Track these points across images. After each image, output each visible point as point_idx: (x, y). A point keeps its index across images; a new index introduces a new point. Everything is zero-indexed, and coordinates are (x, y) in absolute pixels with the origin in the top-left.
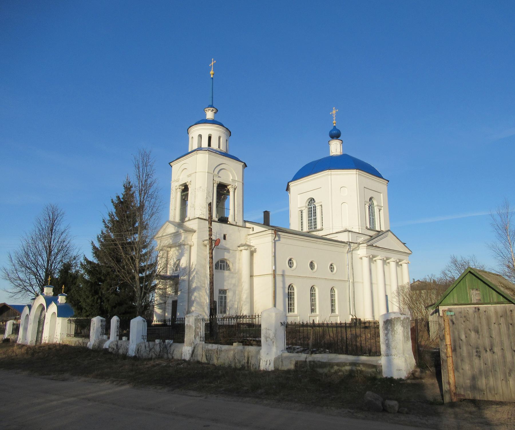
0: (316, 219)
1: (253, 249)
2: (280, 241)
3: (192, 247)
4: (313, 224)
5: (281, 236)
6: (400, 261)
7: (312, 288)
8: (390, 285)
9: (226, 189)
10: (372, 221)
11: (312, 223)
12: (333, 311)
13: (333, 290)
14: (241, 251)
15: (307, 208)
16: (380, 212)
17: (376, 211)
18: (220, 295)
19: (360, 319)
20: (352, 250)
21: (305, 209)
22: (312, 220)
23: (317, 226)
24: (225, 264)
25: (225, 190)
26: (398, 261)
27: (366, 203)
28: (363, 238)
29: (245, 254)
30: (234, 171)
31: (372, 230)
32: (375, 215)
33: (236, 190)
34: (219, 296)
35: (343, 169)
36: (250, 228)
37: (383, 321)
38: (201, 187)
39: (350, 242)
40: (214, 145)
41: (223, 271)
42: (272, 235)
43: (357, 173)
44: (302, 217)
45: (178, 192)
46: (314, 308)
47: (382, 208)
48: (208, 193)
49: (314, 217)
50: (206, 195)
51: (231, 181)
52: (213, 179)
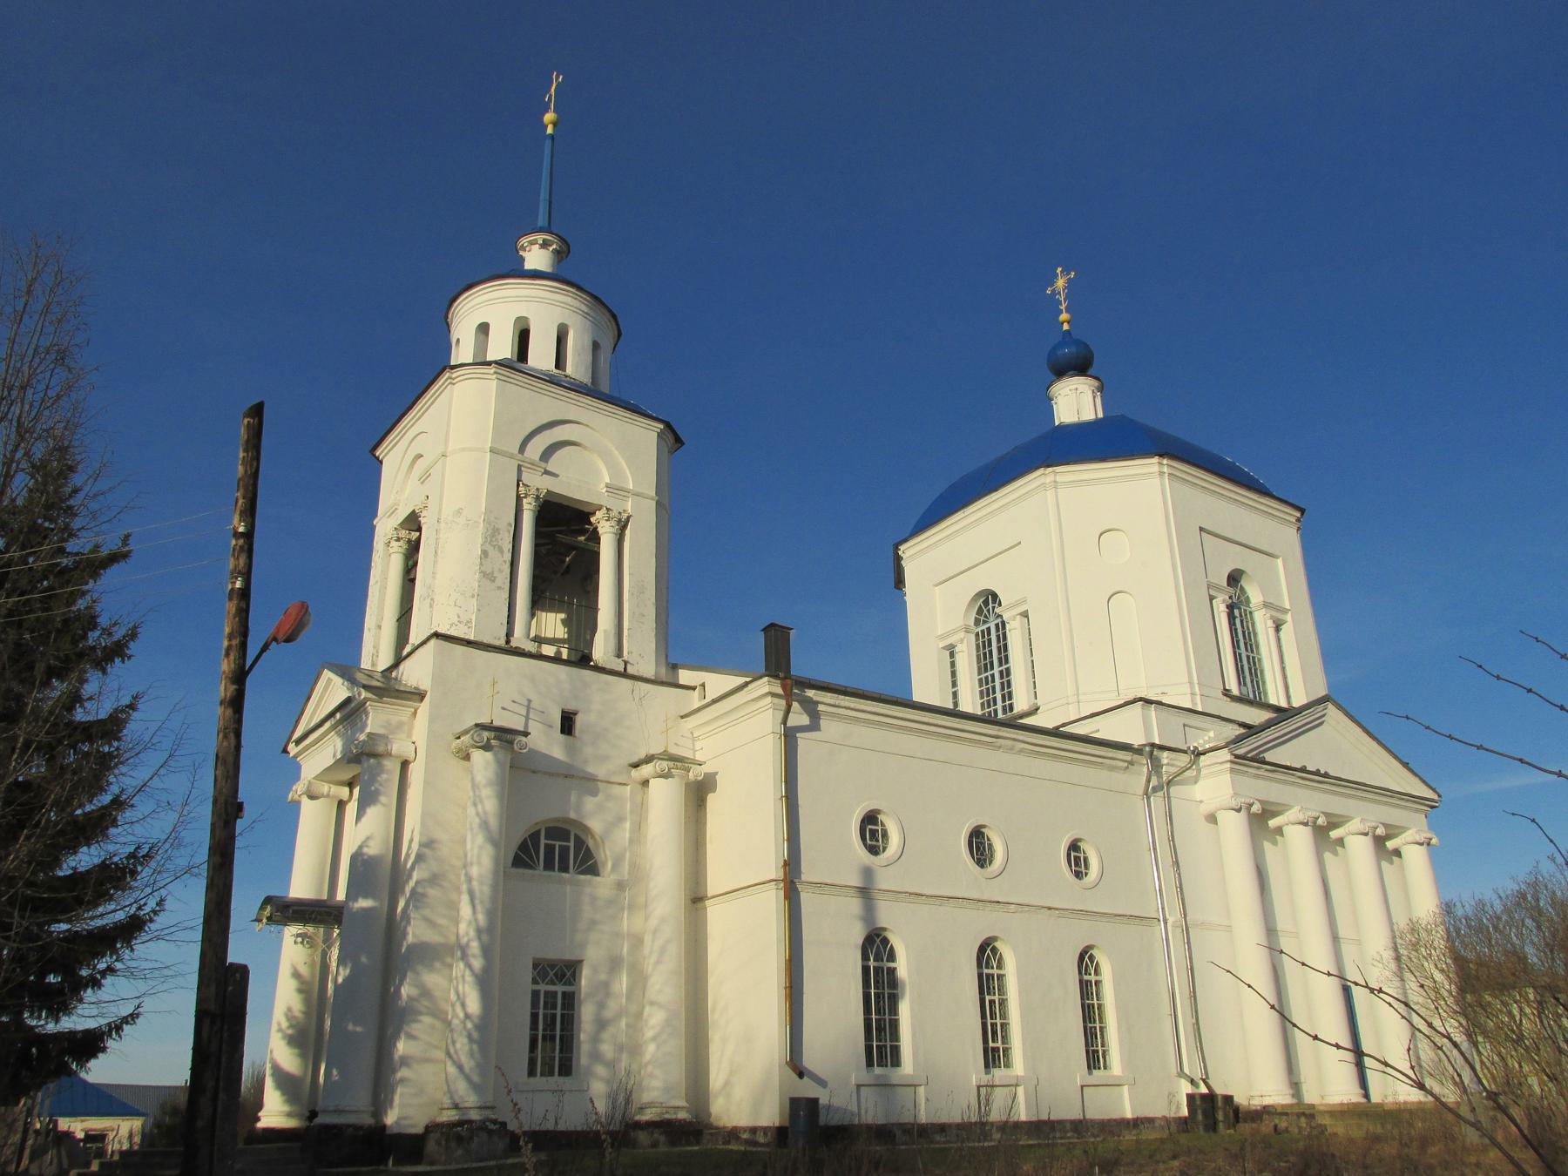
0: (1008, 671)
1: (696, 773)
2: (819, 730)
3: (411, 766)
4: (999, 696)
5: (821, 707)
6: (1388, 837)
7: (987, 952)
8: (1359, 942)
9: (587, 530)
10: (1248, 666)
11: (994, 692)
12: (1095, 1059)
13: (1092, 962)
14: (645, 783)
15: (973, 637)
16: (1282, 634)
17: (1260, 628)
18: (543, 988)
19: (1228, 1099)
20: (1169, 783)
21: (962, 641)
22: (993, 681)
23: (1014, 701)
24: (572, 844)
25: (583, 532)
26: (1380, 831)
27: (1213, 593)
28: (1212, 734)
29: (664, 797)
30: (616, 453)
31: (1250, 703)
32: (1257, 647)
33: (628, 532)
34: (535, 994)
35: (1103, 459)
36: (694, 688)
37: (605, 855)
38: (459, 512)
39: (1153, 745)
40: (541, 356)
41: (556, 874)
42: (776, 700)
43: (1165, 469)
44: (954, 674)
45: (393, 556)
46: (999, 1044)
47: (1288, 617)
48: (492, 534)
49: (1001, 665)
50: (480, 541)
51: (604, 491)
52: (519, 481)
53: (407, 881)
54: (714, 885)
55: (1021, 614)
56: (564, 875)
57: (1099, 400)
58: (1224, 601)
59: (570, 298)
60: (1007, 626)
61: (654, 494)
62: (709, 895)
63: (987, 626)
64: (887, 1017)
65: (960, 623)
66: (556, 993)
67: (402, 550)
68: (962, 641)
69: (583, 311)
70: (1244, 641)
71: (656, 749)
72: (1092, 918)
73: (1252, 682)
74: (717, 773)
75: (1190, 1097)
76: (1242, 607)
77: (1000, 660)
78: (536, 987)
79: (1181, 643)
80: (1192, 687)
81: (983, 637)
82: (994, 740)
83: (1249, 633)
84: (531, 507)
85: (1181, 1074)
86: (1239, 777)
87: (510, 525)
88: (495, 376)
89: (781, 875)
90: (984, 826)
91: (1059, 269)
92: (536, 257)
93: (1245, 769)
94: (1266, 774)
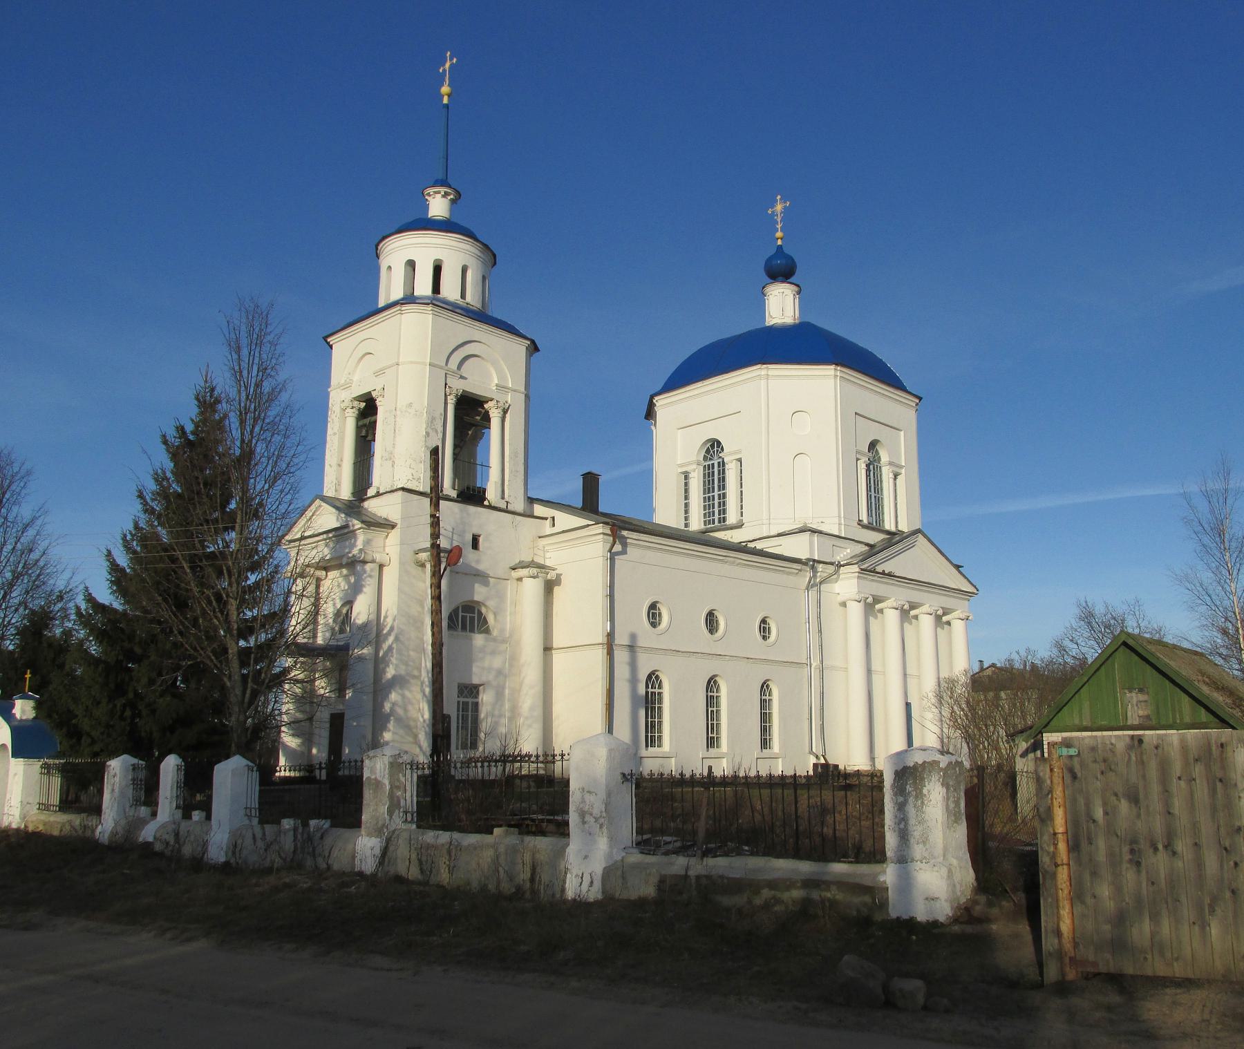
0: (724, 495)
1: (552, 575)
5: (628, 541)
6: (945, 614)
7: (712, 684)
11: (713, 508)
12: (765, 743)
14: (520, 579)
15: (702, 468)
18: (462, 700)
20: (821, 583)
21: (694, 470)
23: (727, 515)
24: (476, 615)
27: (859, 456)
28: (848, 551)
29: (531, 589)
30: (502, 362)
31: (873, 529)
32: (882, 490)
33: (508, 416)
34: (458, 702)
36: (546, 519)
38: (410, 405)
39: (814, 561)
40: (450, 290)
41: (468, 633)
43: (838, 373)
44: (686, 491)
46: (715, 735)
47: (903, 471)
48: (431, 420)
49: (719, 490)
50: (424, 426)
51: (494, 388)
52: (446, 384)
53: (384, 641)
54: (556, 643)
55: (737, 460)
56: (464, 634)
57: (797, 300)
58: (865, 462)
59: (468, 246)
60: (727, 466)
61: (523, 389)
62: (554, 646)
63: (712, 462)
64: (656, 720)
65: (694, 458)
66: (468, 702)
67: (355, 415)
68: (694, 470)
69: (477, 255)
70: (874, 486)
71: (528, 559)
72: (770, 663)
73: (876, 513)
74: (561, 574)
75: (815, 765)
76: (875, 464)
77: (719, 486)
78: (459, 699)
79: (836, 493)
80: (840, 520)
81: (709, 469)
82: (724, 558)
83: (878, 481)
84: (453, 402)
85: (811, 752)
86: (862, 582)
87: (441, 414)
88: (431, 312)
89: (605, 641)
90: (714, 610)
91: (779, 197)
92: (438, 206)
93: (866, 576)
94: (879, 579)
